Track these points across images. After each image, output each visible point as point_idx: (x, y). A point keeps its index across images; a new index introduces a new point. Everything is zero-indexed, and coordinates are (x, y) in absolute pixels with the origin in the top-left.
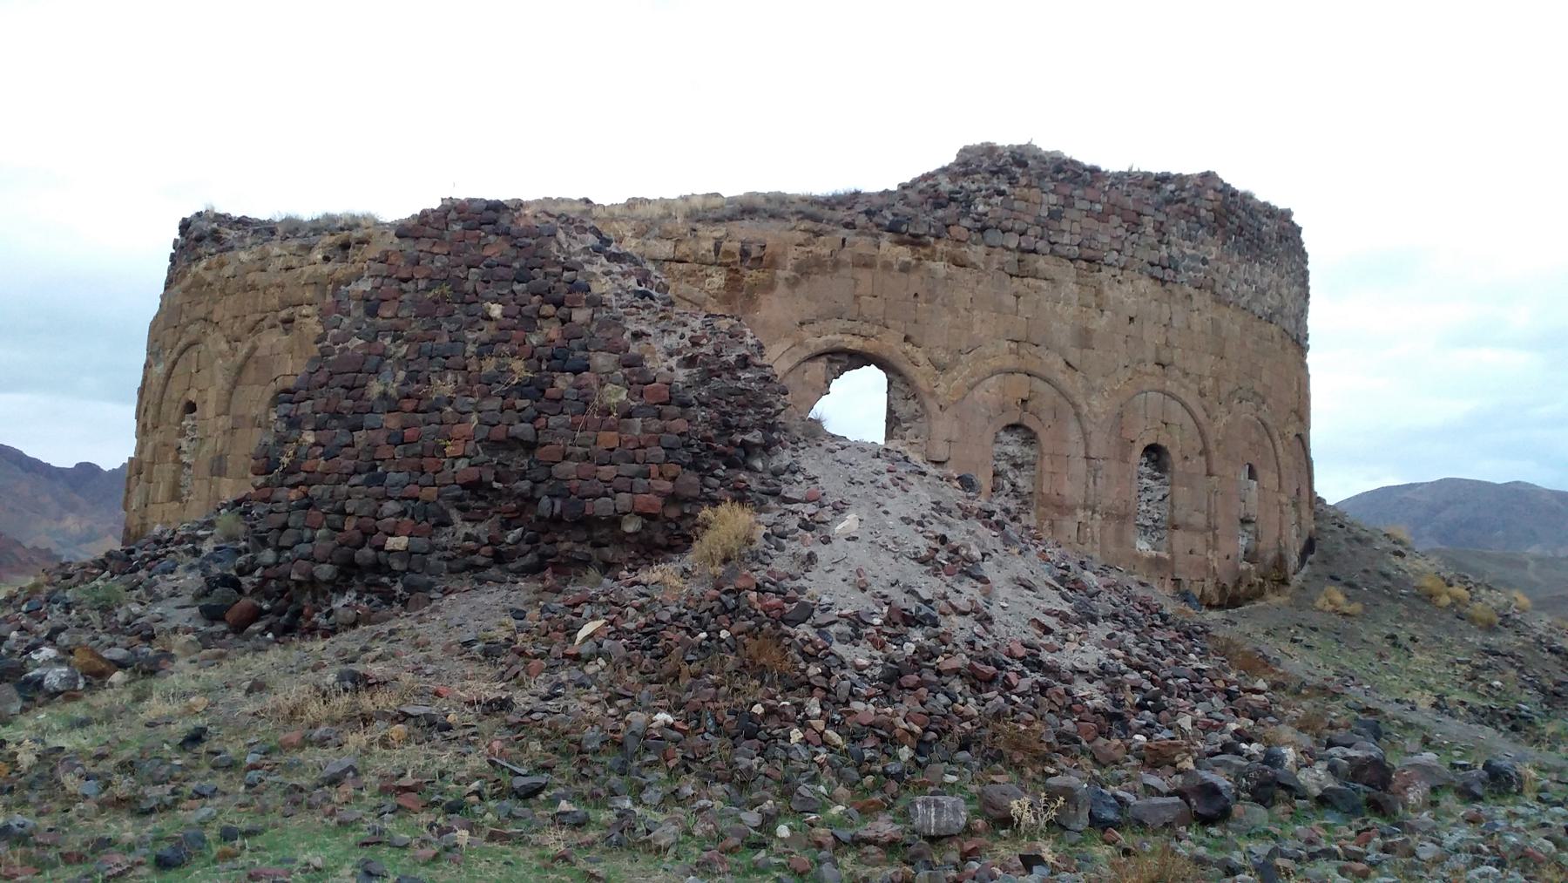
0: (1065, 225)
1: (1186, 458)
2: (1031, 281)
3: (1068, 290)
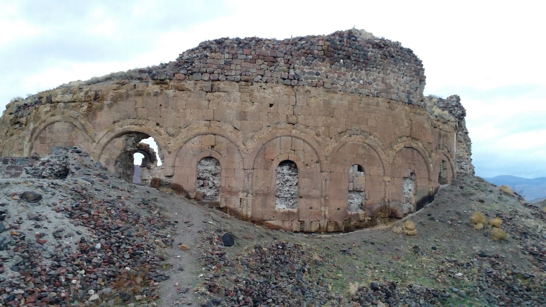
0: (233, 67)
1: (307, 165)
2: (217, 93)
3: (234, 96)
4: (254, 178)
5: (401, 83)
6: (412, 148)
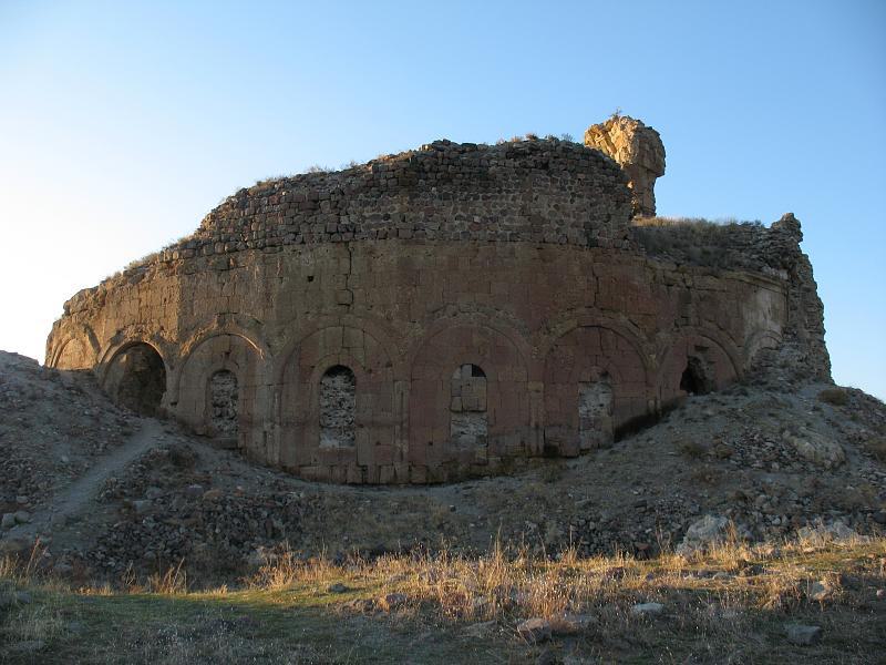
1: (370, 371)
4: (283, 397)
5: (567, 211)
6: (599, 326)
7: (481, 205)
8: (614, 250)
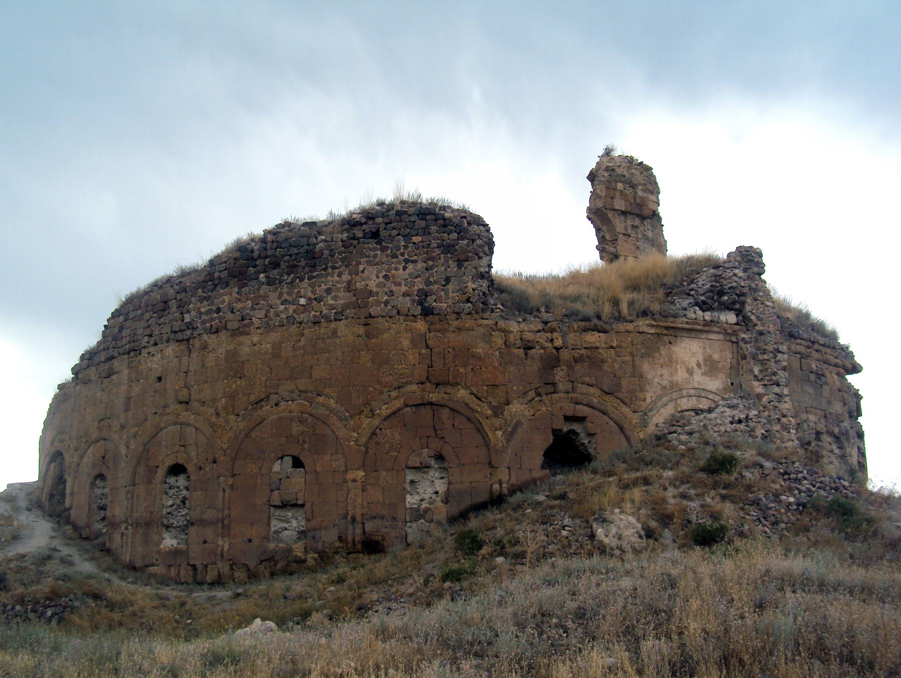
6: (431, 404)
7: (307, 285)
8: (454, 316)
